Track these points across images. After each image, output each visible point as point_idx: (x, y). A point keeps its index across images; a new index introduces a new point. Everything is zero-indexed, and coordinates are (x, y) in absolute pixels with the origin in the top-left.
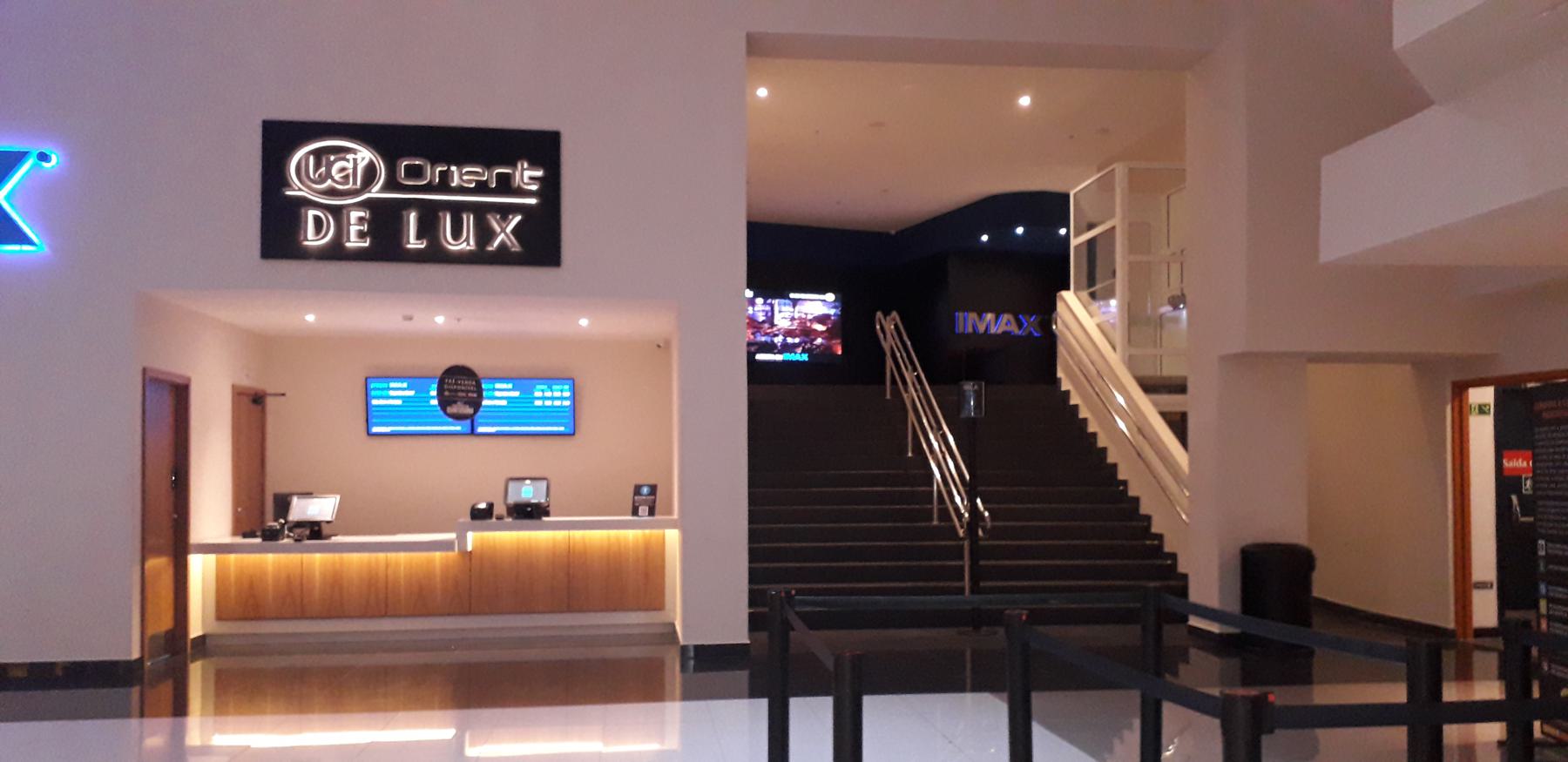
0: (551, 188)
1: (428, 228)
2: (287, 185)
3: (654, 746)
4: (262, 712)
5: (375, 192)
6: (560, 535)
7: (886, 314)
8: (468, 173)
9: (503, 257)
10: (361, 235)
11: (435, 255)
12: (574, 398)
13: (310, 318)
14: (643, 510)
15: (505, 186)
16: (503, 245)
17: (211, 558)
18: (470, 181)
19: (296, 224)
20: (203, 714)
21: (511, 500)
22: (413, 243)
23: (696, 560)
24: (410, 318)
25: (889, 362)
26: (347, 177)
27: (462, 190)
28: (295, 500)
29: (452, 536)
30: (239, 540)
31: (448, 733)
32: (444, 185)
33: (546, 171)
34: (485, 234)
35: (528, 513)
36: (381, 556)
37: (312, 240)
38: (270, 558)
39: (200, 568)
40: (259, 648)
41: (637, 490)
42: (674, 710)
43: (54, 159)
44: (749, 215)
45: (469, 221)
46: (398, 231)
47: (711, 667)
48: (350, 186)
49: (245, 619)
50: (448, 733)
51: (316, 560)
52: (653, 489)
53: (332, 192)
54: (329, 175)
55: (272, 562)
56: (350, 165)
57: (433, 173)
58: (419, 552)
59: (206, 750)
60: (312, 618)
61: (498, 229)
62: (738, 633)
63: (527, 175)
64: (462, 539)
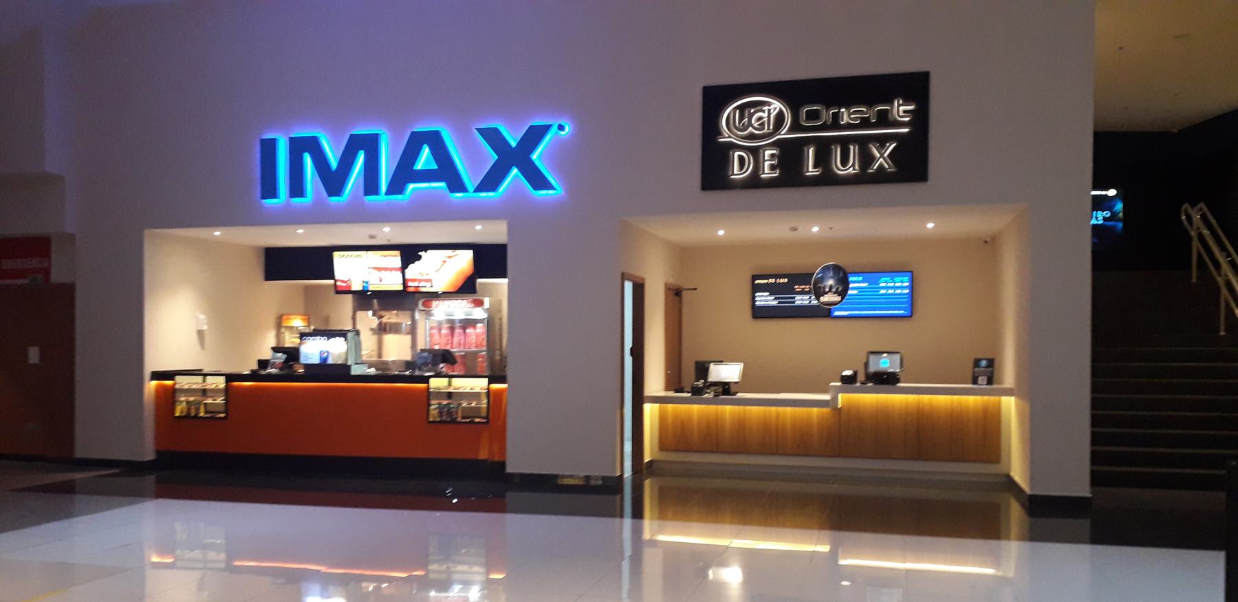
0: (920, 120)
1: (823, 159)
2: (720, 134)
3: (990, 571)
4: (722, 522)
5: (783, 134)
6: (911, 398)
7: (1193, 206)
8: (855, 112)
9: (881, 177)
10: (773, 168)
11: (828, 179)
12: (912, 287)
13: (721, 233)
14: (982, 380)
15: (884, 119)
16: (881, 166)
17: (657, 406)
18: (856, 119)
19: (725, 162)
20: (651, 518)
21: (872, 369)
22: (811, 171)
23: (1024, 422)
24: (795, 229)
25: (1196, 244)
26: (762, 124)
27: (849, 127)
28: (712, 366)
29: (827, 397)
30: (671, 394)
31: (825, 548)
32: (835, 124)
33: (917, 105)
34: (866, 159)
35: (885, 380)
36: (773, 409)
37: (737, 173)
38: (695, 408)
39: (649, 410)
40: (689, 472)
41: (977, 363)
42: (1013, 549)
43: (567, 129)
44: (1095, 126)
45: (853, 150)
46: (800, 160)
47: (1050, 516)
48: (766, 130)
49: (677, 451)
50: (825, 548)
51: (728, 410)
52: (991, 363)
53: (752, 137)
54: (750, 124)
55: (696, 410)
56: (766, 115)
57: (827, 115)
58: (801, 406)
59: (653, 543)
60: (722, 452)
61: (878, 155)
62: (1080, 487)
63: (901, 109)
64: (835, 399)
